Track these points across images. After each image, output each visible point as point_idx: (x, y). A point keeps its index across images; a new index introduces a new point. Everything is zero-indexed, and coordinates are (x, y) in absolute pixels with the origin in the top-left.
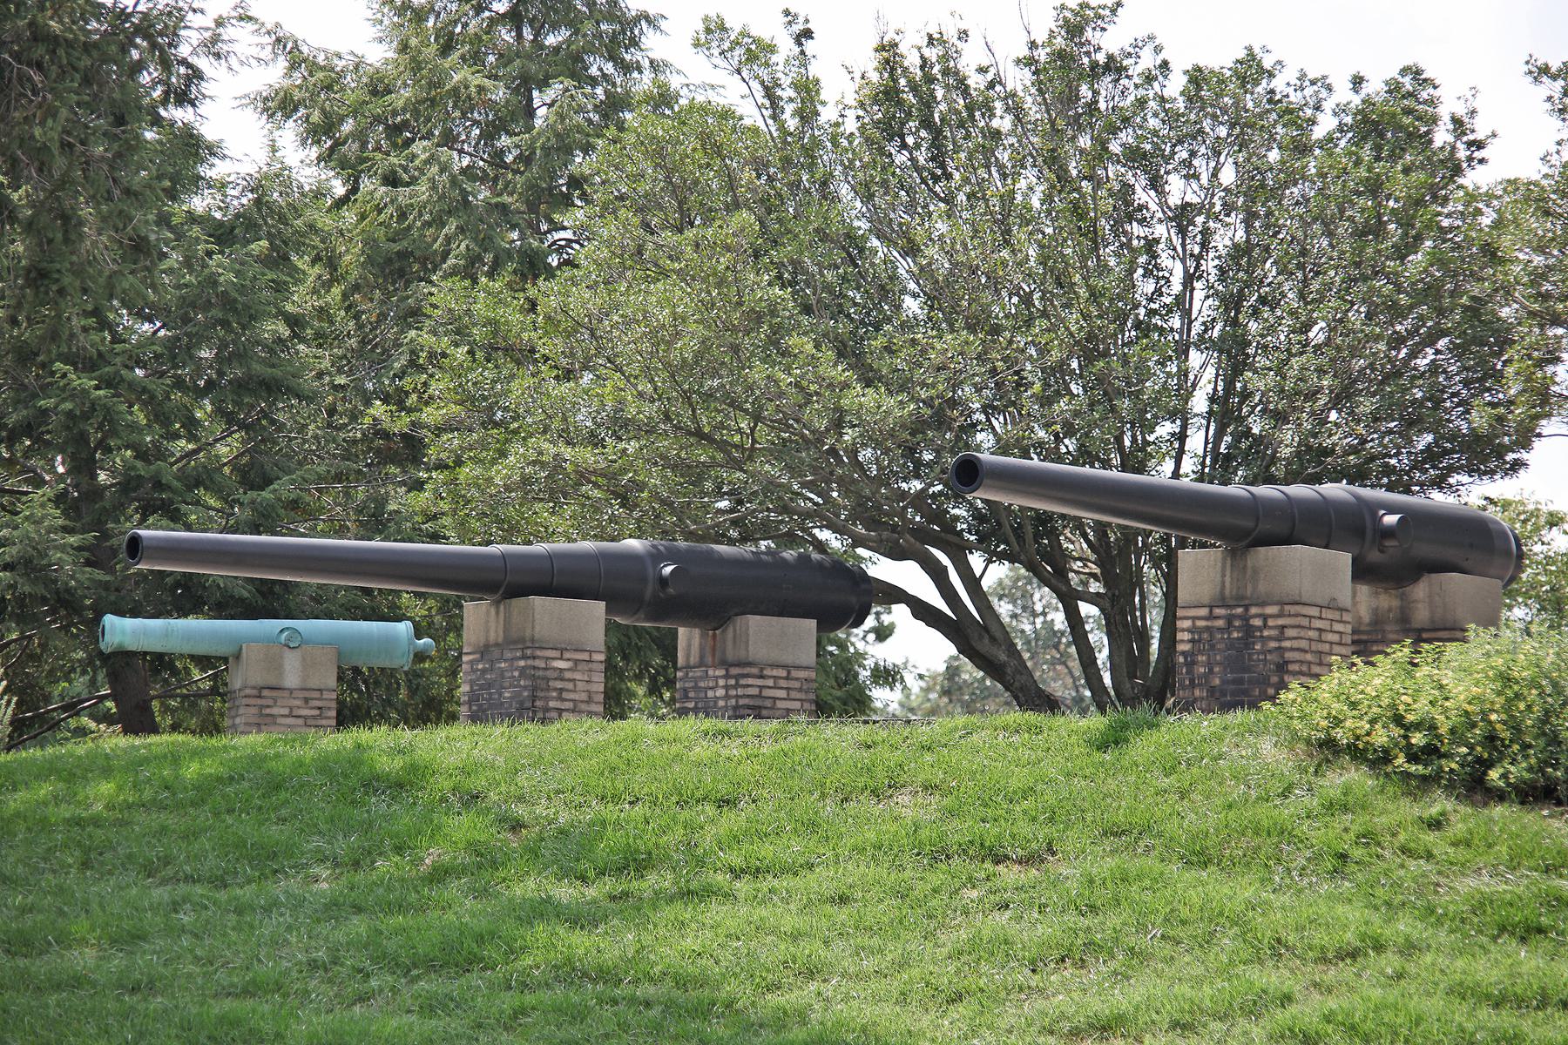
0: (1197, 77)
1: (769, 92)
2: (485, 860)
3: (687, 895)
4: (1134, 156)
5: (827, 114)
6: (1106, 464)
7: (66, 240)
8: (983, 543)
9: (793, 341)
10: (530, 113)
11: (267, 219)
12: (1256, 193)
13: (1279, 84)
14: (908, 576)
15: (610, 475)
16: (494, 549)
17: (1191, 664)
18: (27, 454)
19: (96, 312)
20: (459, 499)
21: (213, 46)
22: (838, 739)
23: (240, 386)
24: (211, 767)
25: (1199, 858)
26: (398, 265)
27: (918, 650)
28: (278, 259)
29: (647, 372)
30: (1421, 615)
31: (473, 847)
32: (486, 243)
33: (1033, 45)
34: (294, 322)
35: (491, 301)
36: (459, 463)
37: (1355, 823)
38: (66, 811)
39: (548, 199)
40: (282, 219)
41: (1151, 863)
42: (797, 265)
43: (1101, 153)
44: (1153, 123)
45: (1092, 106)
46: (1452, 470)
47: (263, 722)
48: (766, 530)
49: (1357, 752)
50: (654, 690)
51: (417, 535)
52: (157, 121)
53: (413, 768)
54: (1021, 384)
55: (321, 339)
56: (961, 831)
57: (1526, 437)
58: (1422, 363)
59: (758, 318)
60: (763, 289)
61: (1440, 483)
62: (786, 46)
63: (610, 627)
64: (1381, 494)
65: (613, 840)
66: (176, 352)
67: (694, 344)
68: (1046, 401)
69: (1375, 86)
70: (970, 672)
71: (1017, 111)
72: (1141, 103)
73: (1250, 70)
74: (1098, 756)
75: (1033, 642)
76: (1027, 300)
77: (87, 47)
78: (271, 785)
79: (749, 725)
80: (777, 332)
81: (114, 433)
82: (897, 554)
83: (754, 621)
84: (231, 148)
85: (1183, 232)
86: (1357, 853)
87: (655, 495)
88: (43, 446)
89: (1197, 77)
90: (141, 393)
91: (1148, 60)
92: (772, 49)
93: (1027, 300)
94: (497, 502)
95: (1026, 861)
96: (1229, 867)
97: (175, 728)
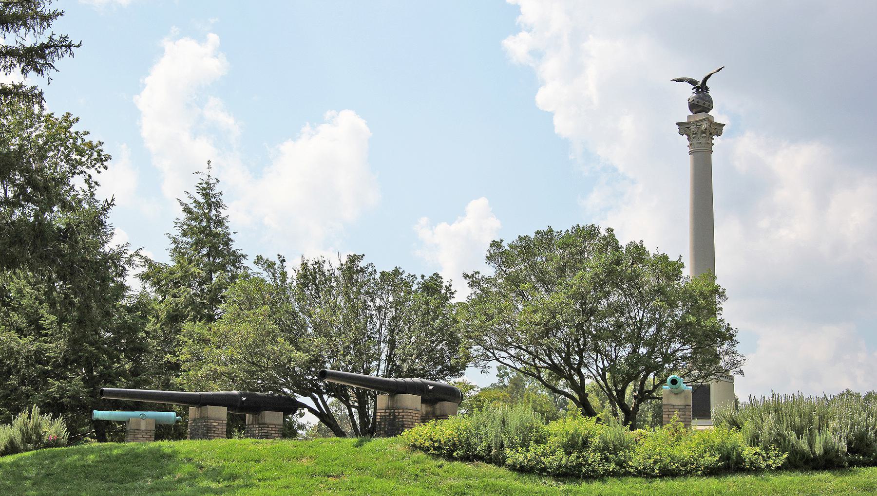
0: (383, 274)
1: (274, 275)
2: (193, 476)
3: (246, 486)
4: (367, 293)
5: (289, 281)
6: (359, 372)
7: (88, 312)
8: (327, 393)
9: (279, 339)
10: (211, 279)
11: (141, 308)
12: (398, 304)
13: (403, 276)
14: (307, 401)
15: (229, 374)
16: (198, 393)
17: (380, 425)
18: (76, 367)
19: (95, 330)
20: (188, 379)
21: (129, 262)
22: (287, 444)
23: (132, 350)
24: (120, 451)
25: (381, 476)
26: (175, 318)
27: (310, 420)
28: (144, 317)
29: (240, 347)
30: (438, 413)
31: (190, 473)
32: (199, 312)
33: (342, 265)
34: (147, 333)
35: (199, 328)
36: (189, 370)
37: (420, 466)
38: (81, 463)
39: (215, 301)
40: (145, 306)
41: (368, 477)
42: (280, 319)
43: (359, 292)
44: (372, 285)
45: (357, 281)
46: (446, 375)
47: (135, 439)
48: (270, 388)
49: (422, 448)
50: (239, 431)
51: (178, 389)
52: (113, 281)
53: (174, 452)
54: (338, 351)
55: (154, 337)
56: (319, 469)
57: (464, 367)
58: (439, 348)
59: (270, 333)
60: (271, 325)
61: (443, 378)
62: (278, 263)
63: (228, 414)
64: (429, 381)
65: (226, 471)
66: (115, 341)
67: (252, 340)
68: (344, 355)
69: (427, 277)
70: (324, 426)
71: (337, 281)
72: (369, 280)
73: (396, 272)
74: (356, 449)
75: (341, 419)
76: (340, 329)
77: (96, 263)
78: (135, 457)
79: (264, 440)
80: (275, 337)
81: (98, 362)
82: (305, 395)
83: (267, 412)
84: (133, 288)
85: (379, 312)
86: (420, 474)
87: (241, 379)
88: (80, 366)
89: (383, 274)
90: (105, 351)
91: (370, 269)
92: (275, 264)
93: (340, 329)
94: (199, 381)
95: (337, 476)
96: (388, 478)
97: (112, 441)
